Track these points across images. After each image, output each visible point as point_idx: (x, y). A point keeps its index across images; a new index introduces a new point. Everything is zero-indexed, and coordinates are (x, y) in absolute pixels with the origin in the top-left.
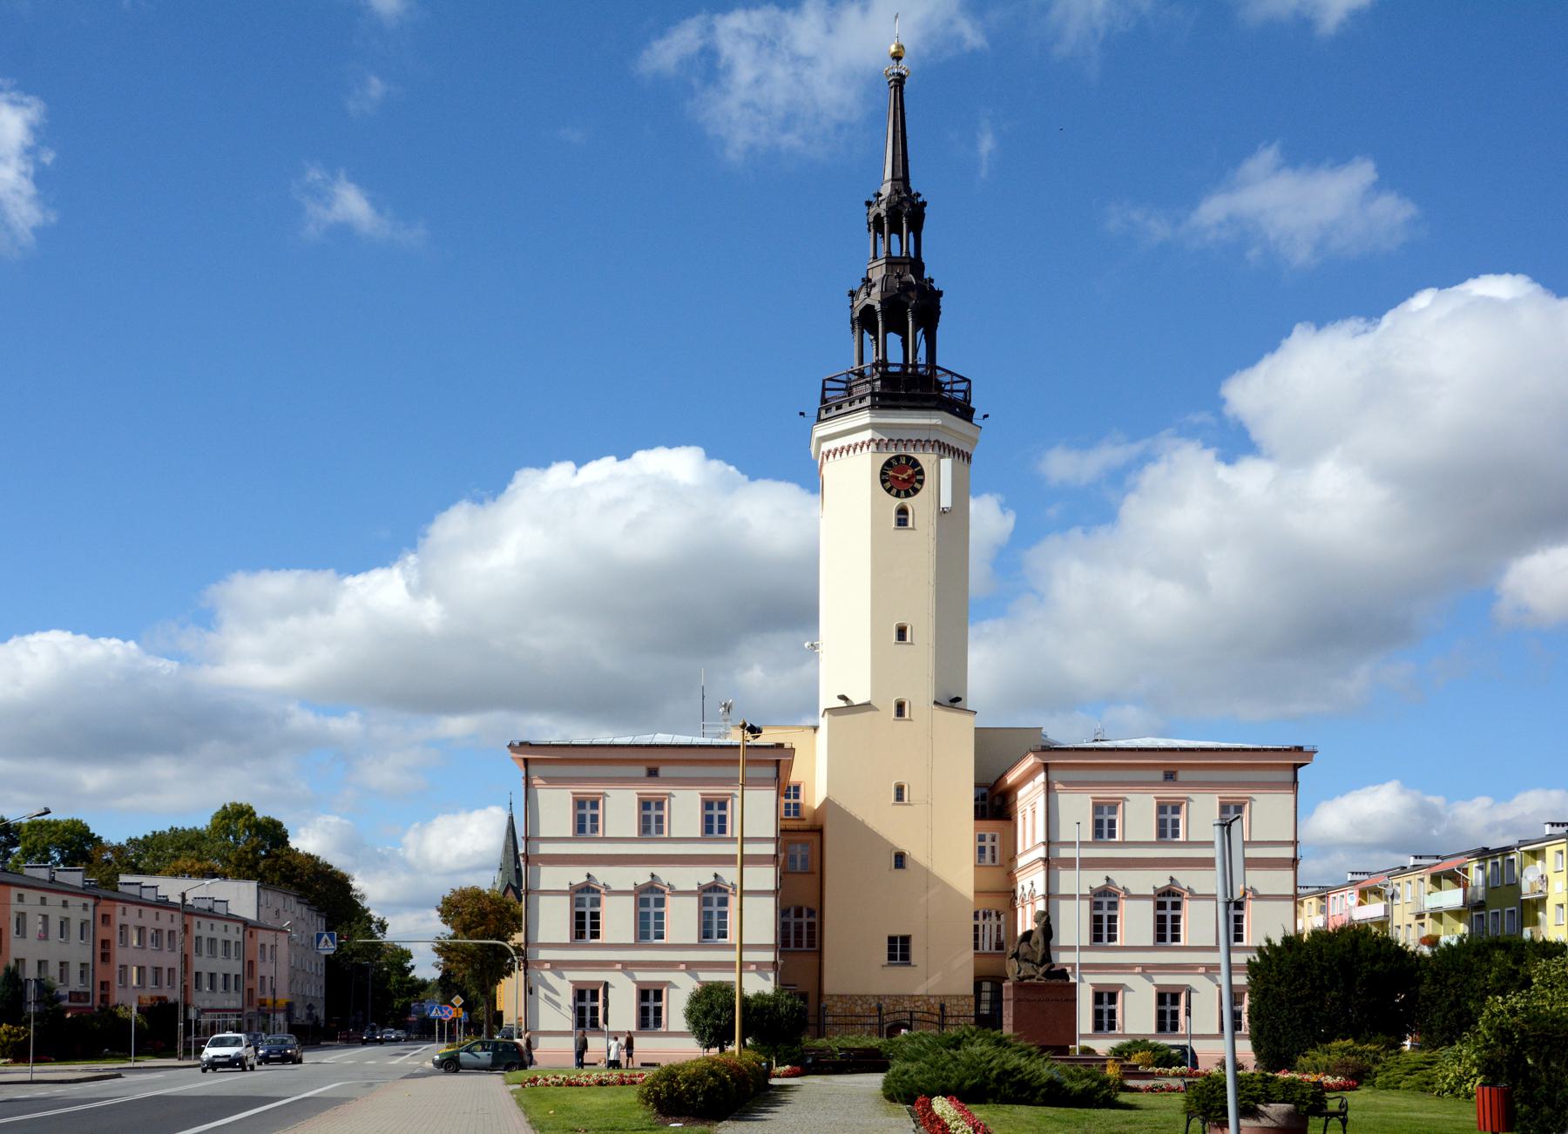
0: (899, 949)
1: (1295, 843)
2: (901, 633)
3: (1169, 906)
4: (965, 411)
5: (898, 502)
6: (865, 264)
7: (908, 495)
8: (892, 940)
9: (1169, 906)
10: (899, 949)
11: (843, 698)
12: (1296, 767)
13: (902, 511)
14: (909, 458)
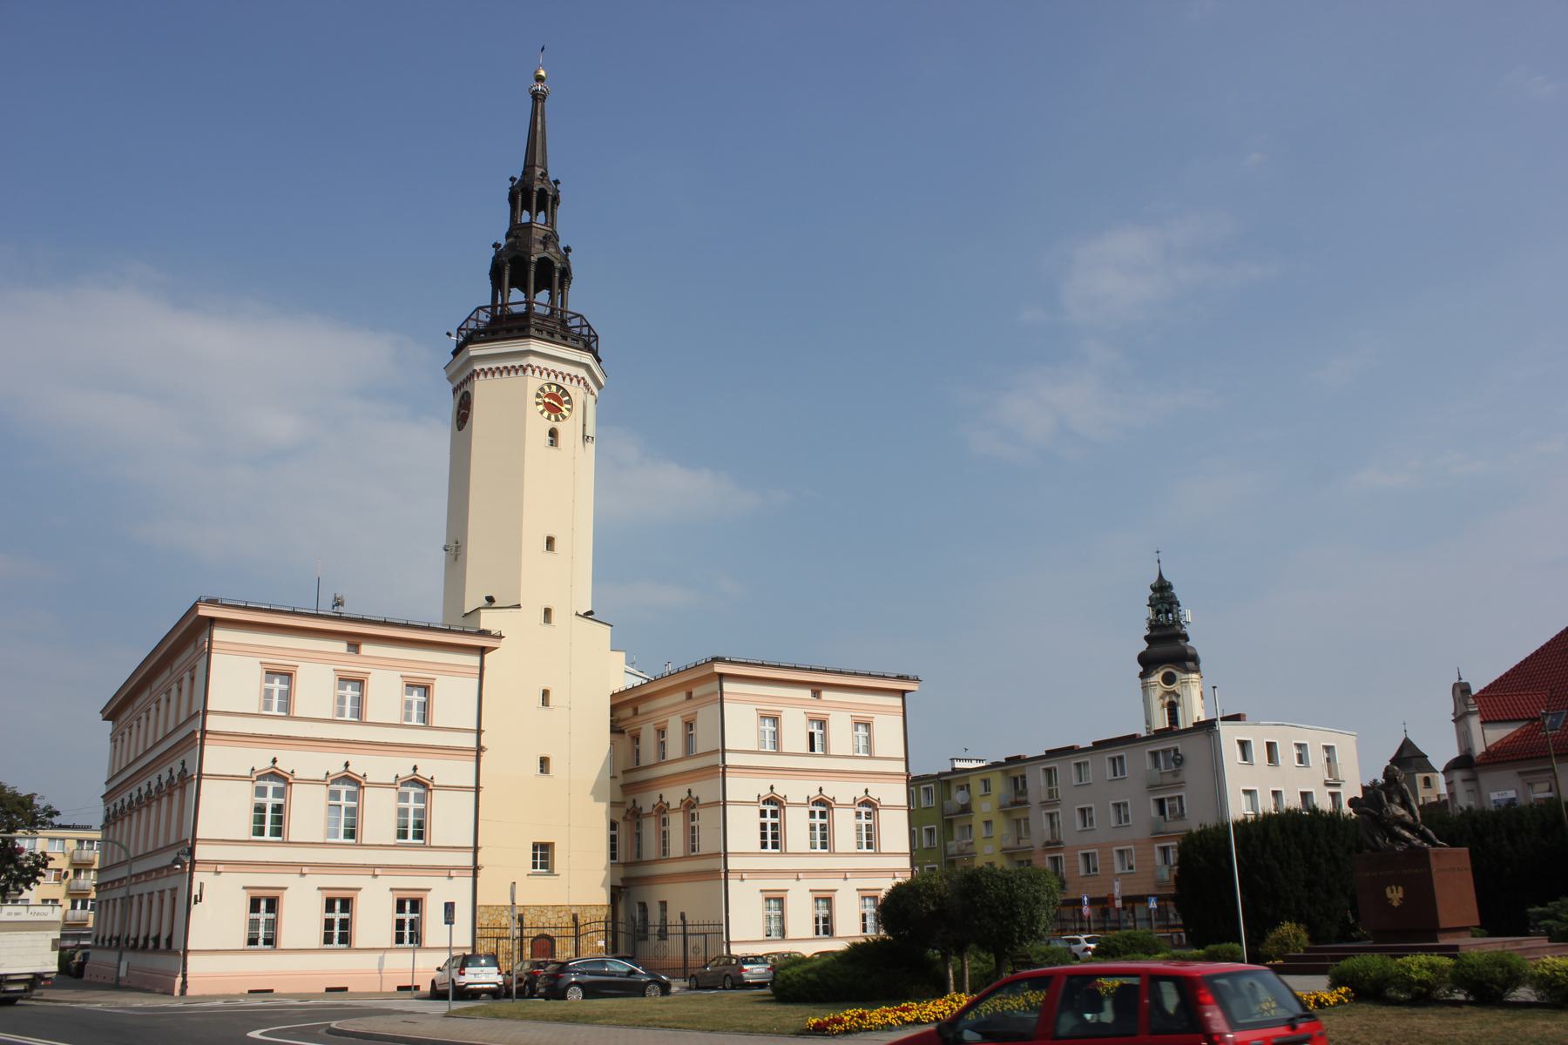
0: (543, 854)
1: (479, 732)
3: (270, 792)
8: (535, 846)
9: (270, 792)
10: (543, 854)
11: (490, 599)
12: (483, 651)
13: (553, 433)
14: (559, 387)
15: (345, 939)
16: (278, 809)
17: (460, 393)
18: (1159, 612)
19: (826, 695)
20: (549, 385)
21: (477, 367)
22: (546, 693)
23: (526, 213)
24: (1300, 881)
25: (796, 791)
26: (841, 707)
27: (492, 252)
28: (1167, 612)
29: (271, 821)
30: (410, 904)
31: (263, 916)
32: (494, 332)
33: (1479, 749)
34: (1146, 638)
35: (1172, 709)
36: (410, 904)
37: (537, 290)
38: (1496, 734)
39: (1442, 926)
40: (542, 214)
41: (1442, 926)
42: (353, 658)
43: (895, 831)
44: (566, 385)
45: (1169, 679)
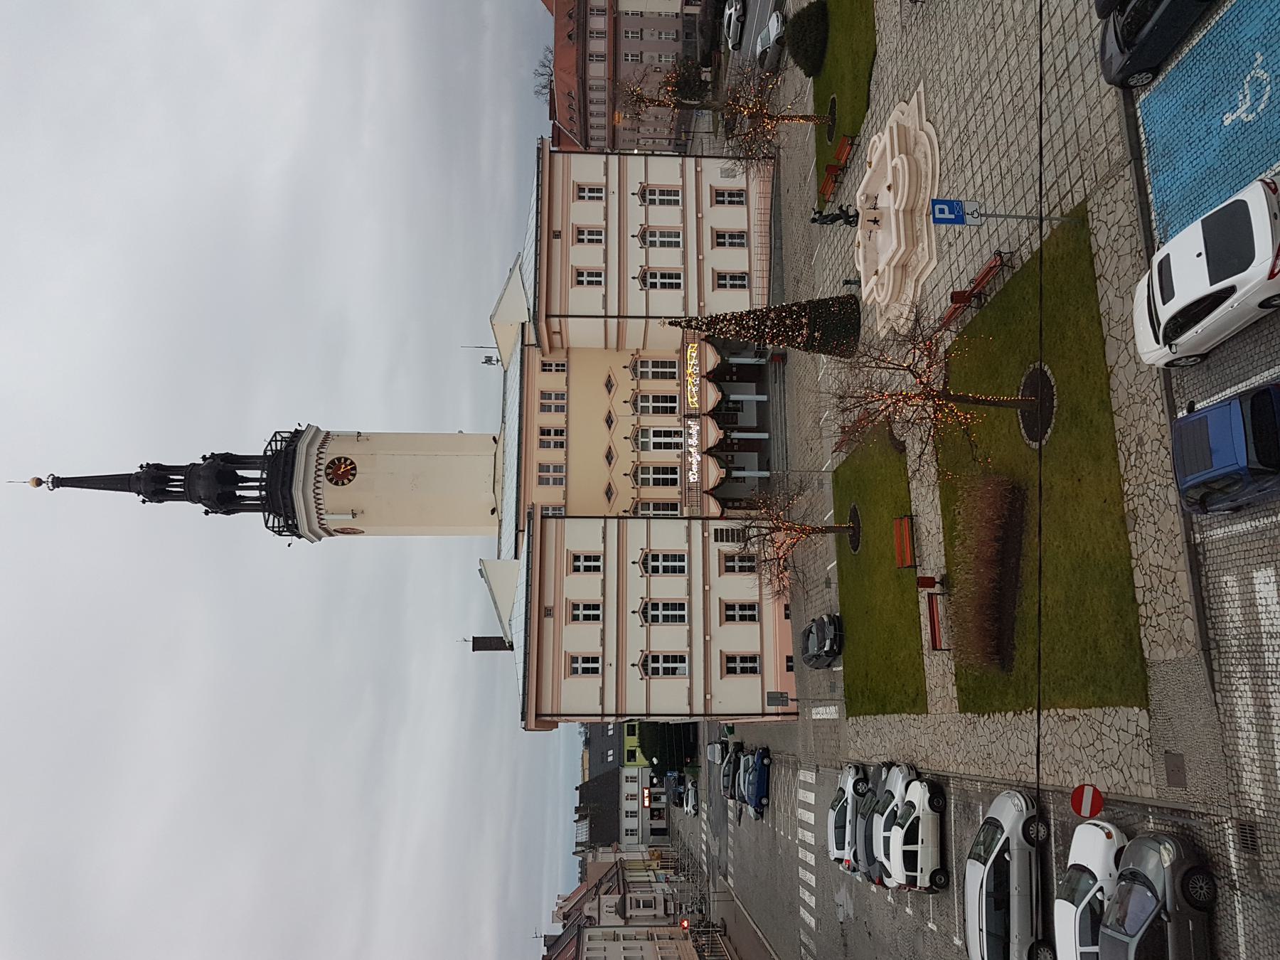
3: (655, 665)
4: (297, 434)
6: (187, 513)
9: (655, 665)
11: (493, 511)
14: (328, 467)
15: (753, 659)
16: (662, 193)
19: (549, 602)
20: (327, 475)
22: (481, 644)
25: (636, 257)
26: (566, 213)
29: (671, 280)
30: (719, 197)
31: (738, 665)
36: (719, 197)
42: (564, 235)
43: (669, 536)
44: (326, 462)
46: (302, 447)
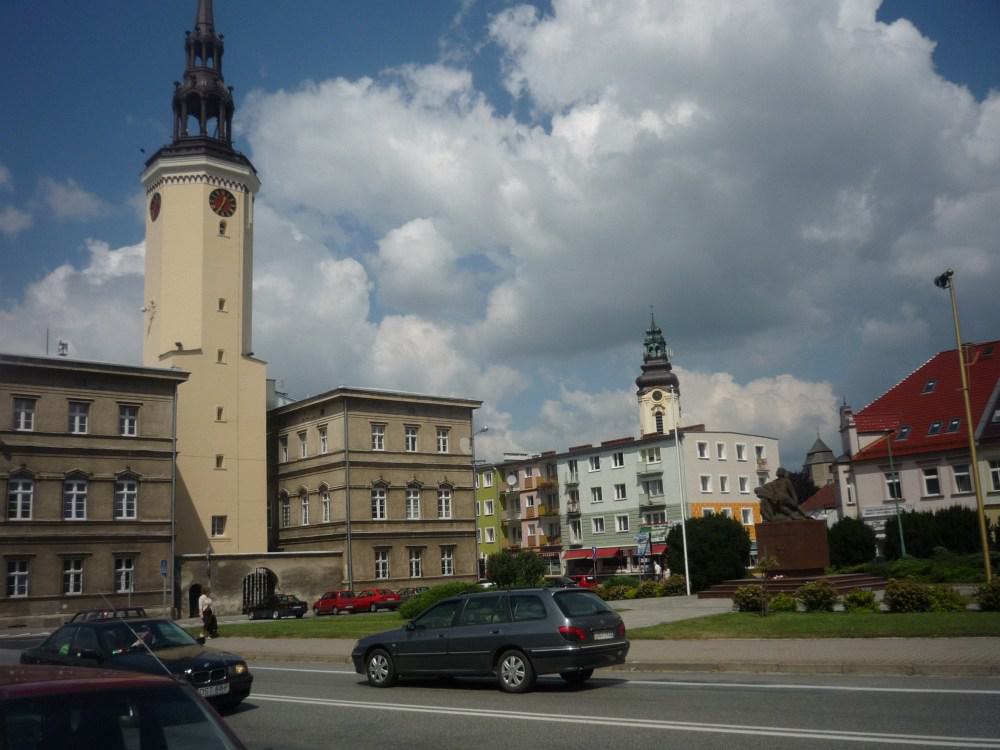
2: (222, 303)
5: (220, 219)
7: (226, 215)
8: (214, 518)
11: (179, 345)
13: (223, 226)
17: (152, 194)
18: (651, 349)
21: (165, 176)
23: (198, 59)
24: (508, 5)
27: (174, 88)
28: (657, 349)
32: (177, 150)
33: (855, 451)
34: (643, 368)
35: (659, 416)
37: (209, 116)
38: (867, 441)
39: (655, 430)
40: (210, 60)
41: (655, 430)
45: (657, 396)
46: (246, 172)
